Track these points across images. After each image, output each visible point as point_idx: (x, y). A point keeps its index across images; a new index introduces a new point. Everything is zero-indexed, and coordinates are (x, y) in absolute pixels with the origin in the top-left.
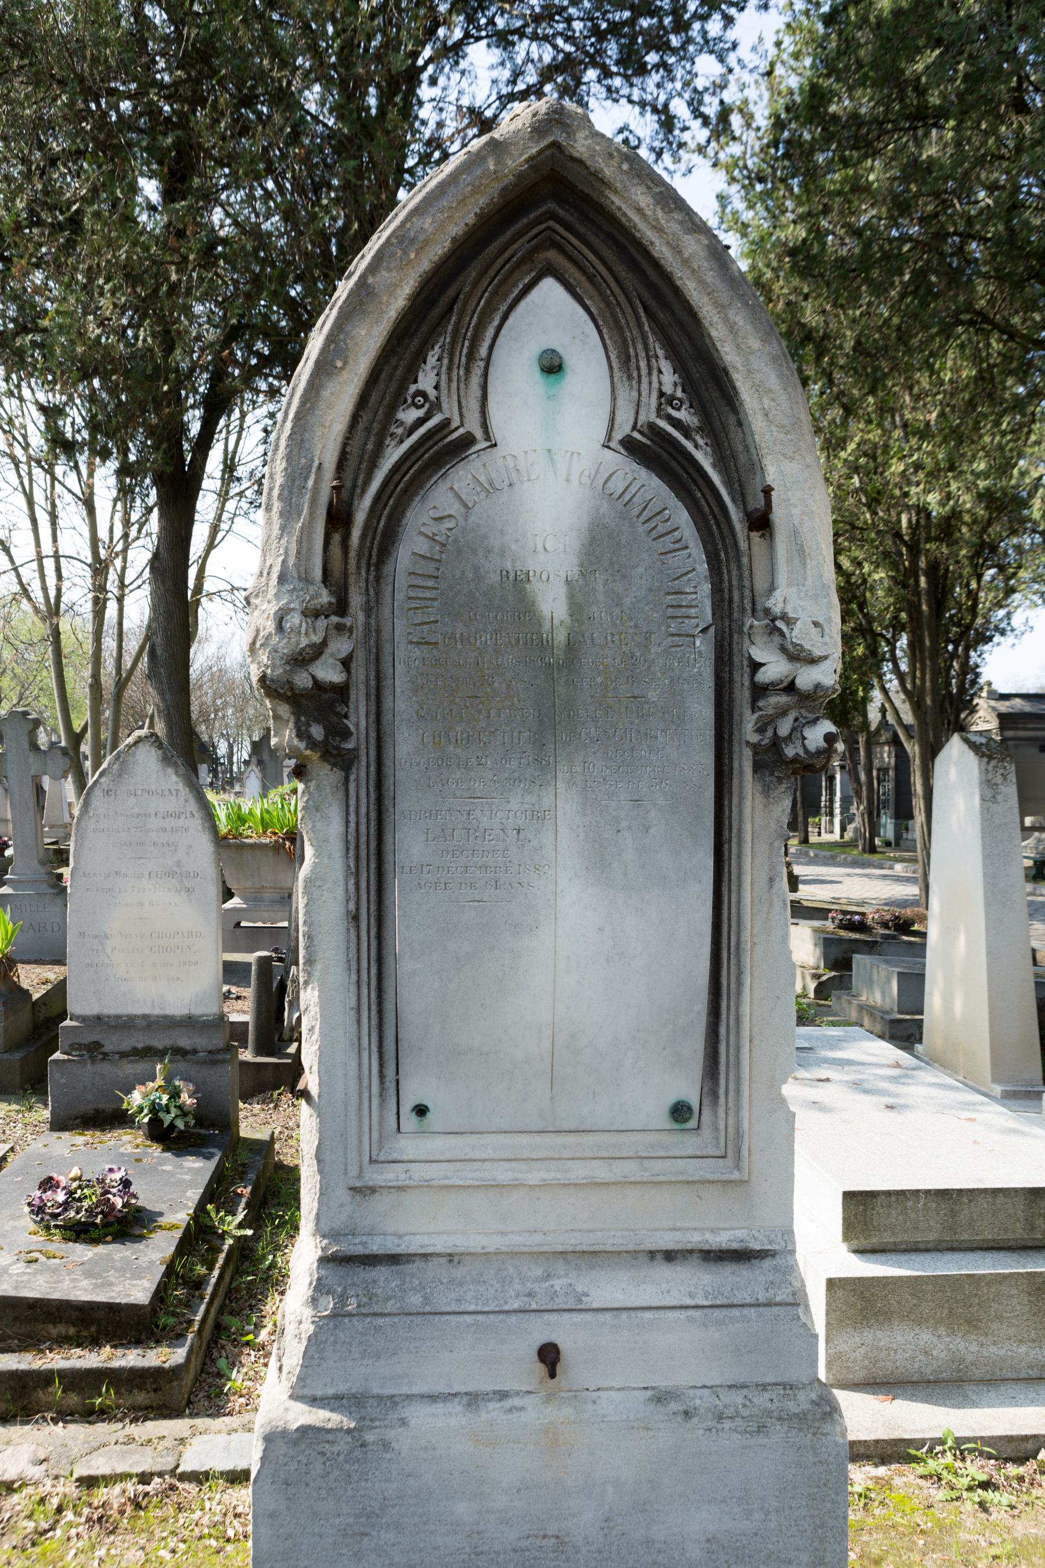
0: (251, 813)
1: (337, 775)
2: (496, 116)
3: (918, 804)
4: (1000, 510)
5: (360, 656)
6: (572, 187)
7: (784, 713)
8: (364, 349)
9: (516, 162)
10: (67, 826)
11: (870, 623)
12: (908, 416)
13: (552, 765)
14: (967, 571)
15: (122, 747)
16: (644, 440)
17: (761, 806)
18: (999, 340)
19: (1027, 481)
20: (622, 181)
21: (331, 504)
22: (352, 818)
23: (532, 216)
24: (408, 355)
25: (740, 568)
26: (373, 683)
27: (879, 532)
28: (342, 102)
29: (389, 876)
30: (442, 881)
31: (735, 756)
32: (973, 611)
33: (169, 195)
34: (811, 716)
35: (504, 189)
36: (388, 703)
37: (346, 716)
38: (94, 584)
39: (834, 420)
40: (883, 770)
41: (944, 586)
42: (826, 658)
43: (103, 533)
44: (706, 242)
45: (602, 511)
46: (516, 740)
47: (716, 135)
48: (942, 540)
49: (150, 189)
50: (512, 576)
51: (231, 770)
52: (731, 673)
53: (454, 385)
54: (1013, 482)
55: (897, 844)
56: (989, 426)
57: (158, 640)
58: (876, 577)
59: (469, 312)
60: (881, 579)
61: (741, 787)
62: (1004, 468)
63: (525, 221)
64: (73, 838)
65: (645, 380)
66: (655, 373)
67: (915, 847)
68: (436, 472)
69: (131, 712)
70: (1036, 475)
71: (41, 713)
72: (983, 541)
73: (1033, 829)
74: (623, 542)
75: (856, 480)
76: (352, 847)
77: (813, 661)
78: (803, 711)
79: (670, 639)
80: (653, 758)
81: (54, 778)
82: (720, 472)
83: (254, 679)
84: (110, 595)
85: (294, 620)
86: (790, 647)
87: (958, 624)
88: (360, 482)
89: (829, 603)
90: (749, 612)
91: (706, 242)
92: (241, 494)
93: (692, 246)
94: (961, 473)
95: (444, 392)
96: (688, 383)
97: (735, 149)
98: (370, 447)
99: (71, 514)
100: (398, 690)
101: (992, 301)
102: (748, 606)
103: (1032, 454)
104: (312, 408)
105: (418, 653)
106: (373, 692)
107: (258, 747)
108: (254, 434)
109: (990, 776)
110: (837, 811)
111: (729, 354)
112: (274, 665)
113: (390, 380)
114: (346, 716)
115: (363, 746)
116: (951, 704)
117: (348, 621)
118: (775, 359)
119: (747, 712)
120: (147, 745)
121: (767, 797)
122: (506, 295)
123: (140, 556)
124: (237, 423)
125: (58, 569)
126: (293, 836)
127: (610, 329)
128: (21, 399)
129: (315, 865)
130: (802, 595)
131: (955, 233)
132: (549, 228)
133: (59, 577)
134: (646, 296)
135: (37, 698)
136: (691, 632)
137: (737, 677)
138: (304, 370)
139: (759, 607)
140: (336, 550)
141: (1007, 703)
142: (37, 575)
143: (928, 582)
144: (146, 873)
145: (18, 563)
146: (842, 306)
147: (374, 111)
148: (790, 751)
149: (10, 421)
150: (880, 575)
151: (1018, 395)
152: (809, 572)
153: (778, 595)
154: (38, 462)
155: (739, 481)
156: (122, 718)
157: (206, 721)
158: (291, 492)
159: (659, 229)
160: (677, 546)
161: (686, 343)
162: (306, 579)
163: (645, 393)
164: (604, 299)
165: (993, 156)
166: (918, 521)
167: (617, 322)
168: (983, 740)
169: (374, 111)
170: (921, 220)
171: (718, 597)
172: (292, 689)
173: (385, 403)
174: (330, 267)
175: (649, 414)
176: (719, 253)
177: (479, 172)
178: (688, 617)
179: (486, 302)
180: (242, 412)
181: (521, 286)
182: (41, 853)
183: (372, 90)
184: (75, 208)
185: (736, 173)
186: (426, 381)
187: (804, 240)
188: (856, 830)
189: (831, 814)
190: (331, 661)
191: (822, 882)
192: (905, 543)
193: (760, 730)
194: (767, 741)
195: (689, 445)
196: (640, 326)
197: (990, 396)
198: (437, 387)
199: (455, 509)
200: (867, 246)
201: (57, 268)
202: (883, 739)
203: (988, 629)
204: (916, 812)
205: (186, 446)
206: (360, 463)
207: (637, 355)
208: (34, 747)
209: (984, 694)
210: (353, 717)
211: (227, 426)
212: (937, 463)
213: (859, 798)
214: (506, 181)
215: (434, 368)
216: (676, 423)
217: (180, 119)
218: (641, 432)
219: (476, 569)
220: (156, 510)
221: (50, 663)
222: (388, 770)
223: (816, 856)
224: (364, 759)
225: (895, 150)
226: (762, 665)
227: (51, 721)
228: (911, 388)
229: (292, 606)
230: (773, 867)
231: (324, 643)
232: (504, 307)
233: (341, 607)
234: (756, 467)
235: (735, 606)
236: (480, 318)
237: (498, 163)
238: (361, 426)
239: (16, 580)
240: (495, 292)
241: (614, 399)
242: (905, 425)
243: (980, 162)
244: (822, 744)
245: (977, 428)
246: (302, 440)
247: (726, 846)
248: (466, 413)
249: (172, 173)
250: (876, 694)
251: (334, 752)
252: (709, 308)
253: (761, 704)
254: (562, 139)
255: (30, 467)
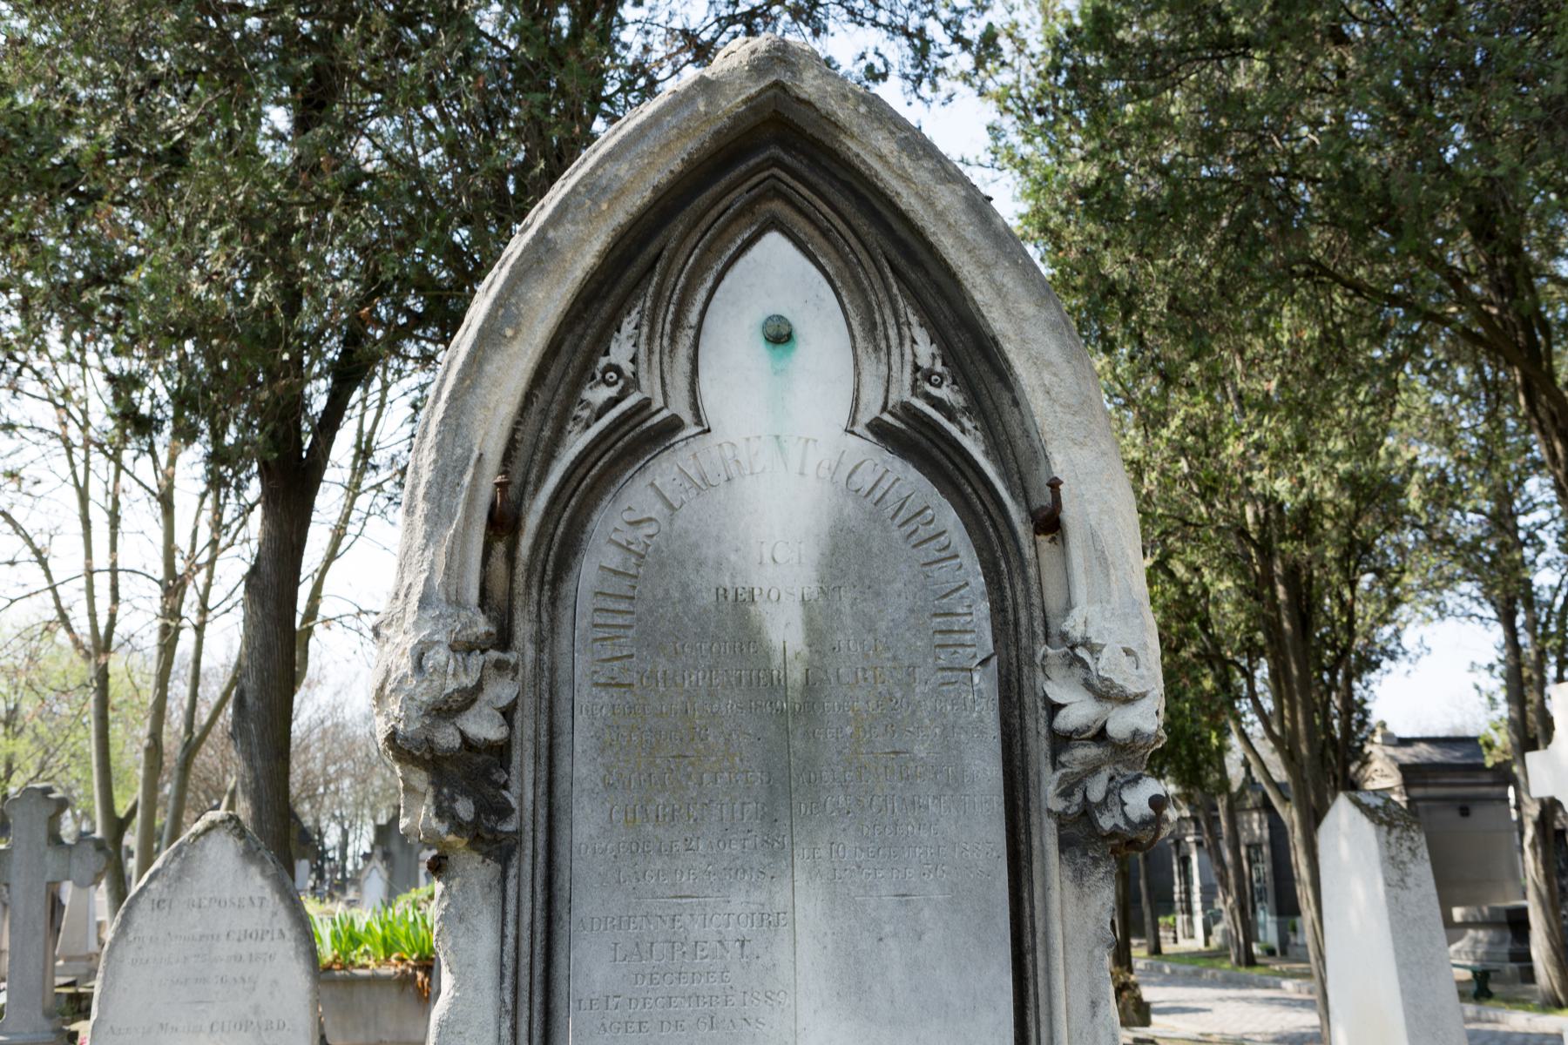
0: (368, 930)
1: (491, 869)
2: (714, 40)
3: (1304, 893)
4: (1370, 499)
5: (528, 703)
6: (799, 131)
7: (1095, 770)
8: (542, 315)
9: (731, 103)
10: (91, 957)
11: (1217, 647)
12: (1240, 385)
13: (788, 848)
14: (1335, 578)
15: (184, 837)
16: (897, 424)
17: (1073, 900)
18: (1345, 295)
19: (1399, 463)
20: (859, 125)
21: (493, 505)
22: (510, 930)
23: (752, 162)
24: (597, 323)
25: (1026, 580)
26: (544, 739)
27: (1218, 529)
28: (527, 23)
29: (560, 1013)
30: (636, 1018)
31: (1035, 830)
32: (1350, 628)
33: (302, 124)
34: (1131, 774)
35: (718, 132)
36: (563, 767)
37: (506, 786)
38: (163, 608)
39: (1148, 391)
40: (1254, 847)
41: (1309, 597)
42: (1144, 695)
43: (182, 540)
44: (963, 193)
45: (846, 512)
46: (738, 815)
47: (980, 63)
48: (1300, 538)
49: (279, 117)
50: (731, 596)
51: (344, 869)
52: (1022, 717)
53: (656, 358)
54: (1381, 465)
55: (1284, 952)
56: (1342, 398)
57: (250, 684)
58: (1222, 587)
59: (675, 272)
60: (1228, 589)
61: (1044, 873)
62: (1367, 446)
63: (743, 168)
64: (100, 975)
65: (895, 352)
66: (908, 343)
67: (1307, 955)
68: (632, 464)
69: (203, 786)
70: (1409, 456)
71: (69, 790)
72: (1352, 539)
73: (1465, 925)
74: (875, 550)
75: (1183, 464)
76: (509, 974)
77: (1128, 700)
78: (1119, 767)
79: (939, 674)
80: (924, 835)
81: (81, 884)
82: (994, 461)
83: (381, 738)
84: (185, 622)
85: (439, 656)
86: (1096, 682)
87: (1333, 647)
88: (533, 477)
89: (1143, 623)
90: (1041, 636)
91: (963, 193)
92: (378, 487)
93: (946, 197)
94: (1314, 453)
95: (643, 366)
96: (949, 355)
97: (1006, 77)
98: (546, 433)
99: (141, 515)
100: (578, 748)
101: (1330, 251)
102: (1040, 630)
103: (1401, 430)
104: (473, 386)
105: (606, 698)
106: (544, 752)
107: (384, 833)
108: (399, 408)
109: (1394, 852)
110: (1197, 906)
111: (997, 321)
112: (408, 717)
113: (574, 352)
114: (506, 786)
115: (528, 828)
116: (1336, 751)
117: (512, 657)
118: (1054, 326)
119: (1047, 769)
120: (223, 833)
121: (1081, 886)
122: (722, 251)
123: (234, 567)
124: (378, 395)
125: (114, 588)
126: (428, 965)
127: (850, 291)
128: (84, 365)
129: (455, 1001)
130: (1108, 614)
131: (1279, 173)
132: (773, 176)
133: (115, 598)
134: (893, 253)
135: (65, 768)
136: (966, 665)
137: (1030, 723)
138: (465, 338)
139: (1053, 631)
140: (499, 564)
141: (1409, 750)
142: (83, 595)
143: (1288, 592)
144: (207, 1025)
145: (56, 580)
146: (1148, 255)
147: (565, 33)
148: (1106, 822)
149: (66, 393)
150: (1227, 583)
151: (1373, 359)
152: (1113, 586)
153: (1077, 615)
154: (100, 446)
155: (1019, 472)
156: (189, 795)
157: (312, 797)
158: (441, 491)
159: (906, 179)
160: (943, 554)
161: (945, 308)
162: (458, 603)
163: (896, 367)
164: (842, 256)
165: (1313, 89)
166: (1266, 514)
167: (858, 283)
168: (1379, 802)
169: (565, 33)
170: (1235, 158)
171: (1000, 618)
172: (432, 750)
173: (567, 379)
174: (505, 209)
175: (902, 392)
176: (979, 205)
177: (686, 114)
178: (962, 645)
179: (696, 260)
180: (384, 381)
181: (739, 242)
182: (49, 1000)
183: (563, 10)
184: (178, 137)
185: (1009, 103)
186: (620, 353)
187: (1099, 181)
188: (1225, 933)
189: (1189, 911)
190: (487, 710)
191: (1184, 1010)
192: (1254, 543)
193: (1066, 794)
194: (1075, 808)
195: (953, 430)
196: (888, 289)
197: (1339, 360)
198: (634, 360)
199: (656, 510)
200: (1176, 184)
201: (146, 205)
202: (1250, 803)
203: (1372, 652)
204: (1303, 905)
205: (306, 426)
206: (534, 453)
207: (884, 323)
208: (55, 839)
209: (1378, 739)
210: (515, 787)
211: (364, 400)
212: (1283, 442)
213: (1226, 886)
214: (719, 124)
215: (630, 337)
216: (937, 403)
217: (321, 38)
218: (891, 413)
219: (684, 587)
220: (259, 508)
221: (90, 718)
222: (562, 860)
223: (1173, 972)
224: (528, 845)
225: (1198, 80)
226: (1064, 706)
227: (83, 802)
228: (1242, 352)
229: (436, 637)
230: (1094, 986)
231: (479, 687)
232: (718, 266)
233: (503, 638)
234: (1038, 455)
235: (1022, 630)
236: (688, 279)
237: (709, 103)
238: (535, 408)
239: (53, 604)
240: (708, 249)
241: (858, 374)
242: (1240, 397)
243: (1301, 95)
244: (1148, 811)
245: (1327, 400)
246: (458, 425)
247: (1029, 957)
248: (670, 392)
249: (307, 101)
250: (1234, 740)
251: (487, 836)
252: (971, 268)
253: (1063, 758)
254: (786, 78)
255: (87, 452)
